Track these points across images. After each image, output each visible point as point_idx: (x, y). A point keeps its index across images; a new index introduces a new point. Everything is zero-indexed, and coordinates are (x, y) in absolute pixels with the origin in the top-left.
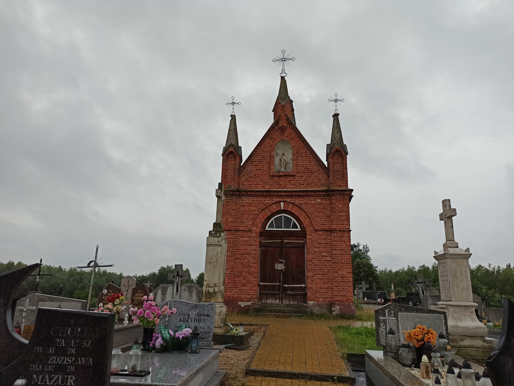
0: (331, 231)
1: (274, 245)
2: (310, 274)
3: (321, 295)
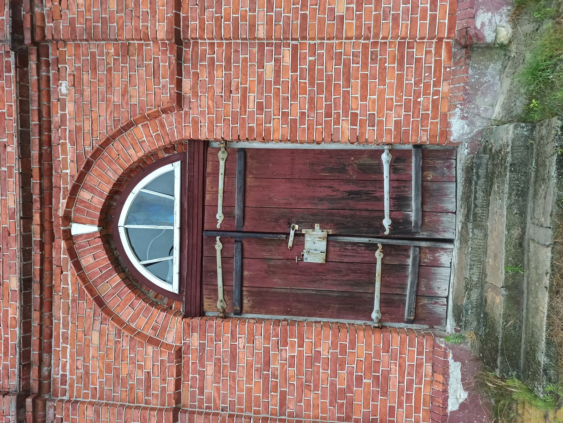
1: (236, 263)
2: (345, 128)
3: (427, 86)
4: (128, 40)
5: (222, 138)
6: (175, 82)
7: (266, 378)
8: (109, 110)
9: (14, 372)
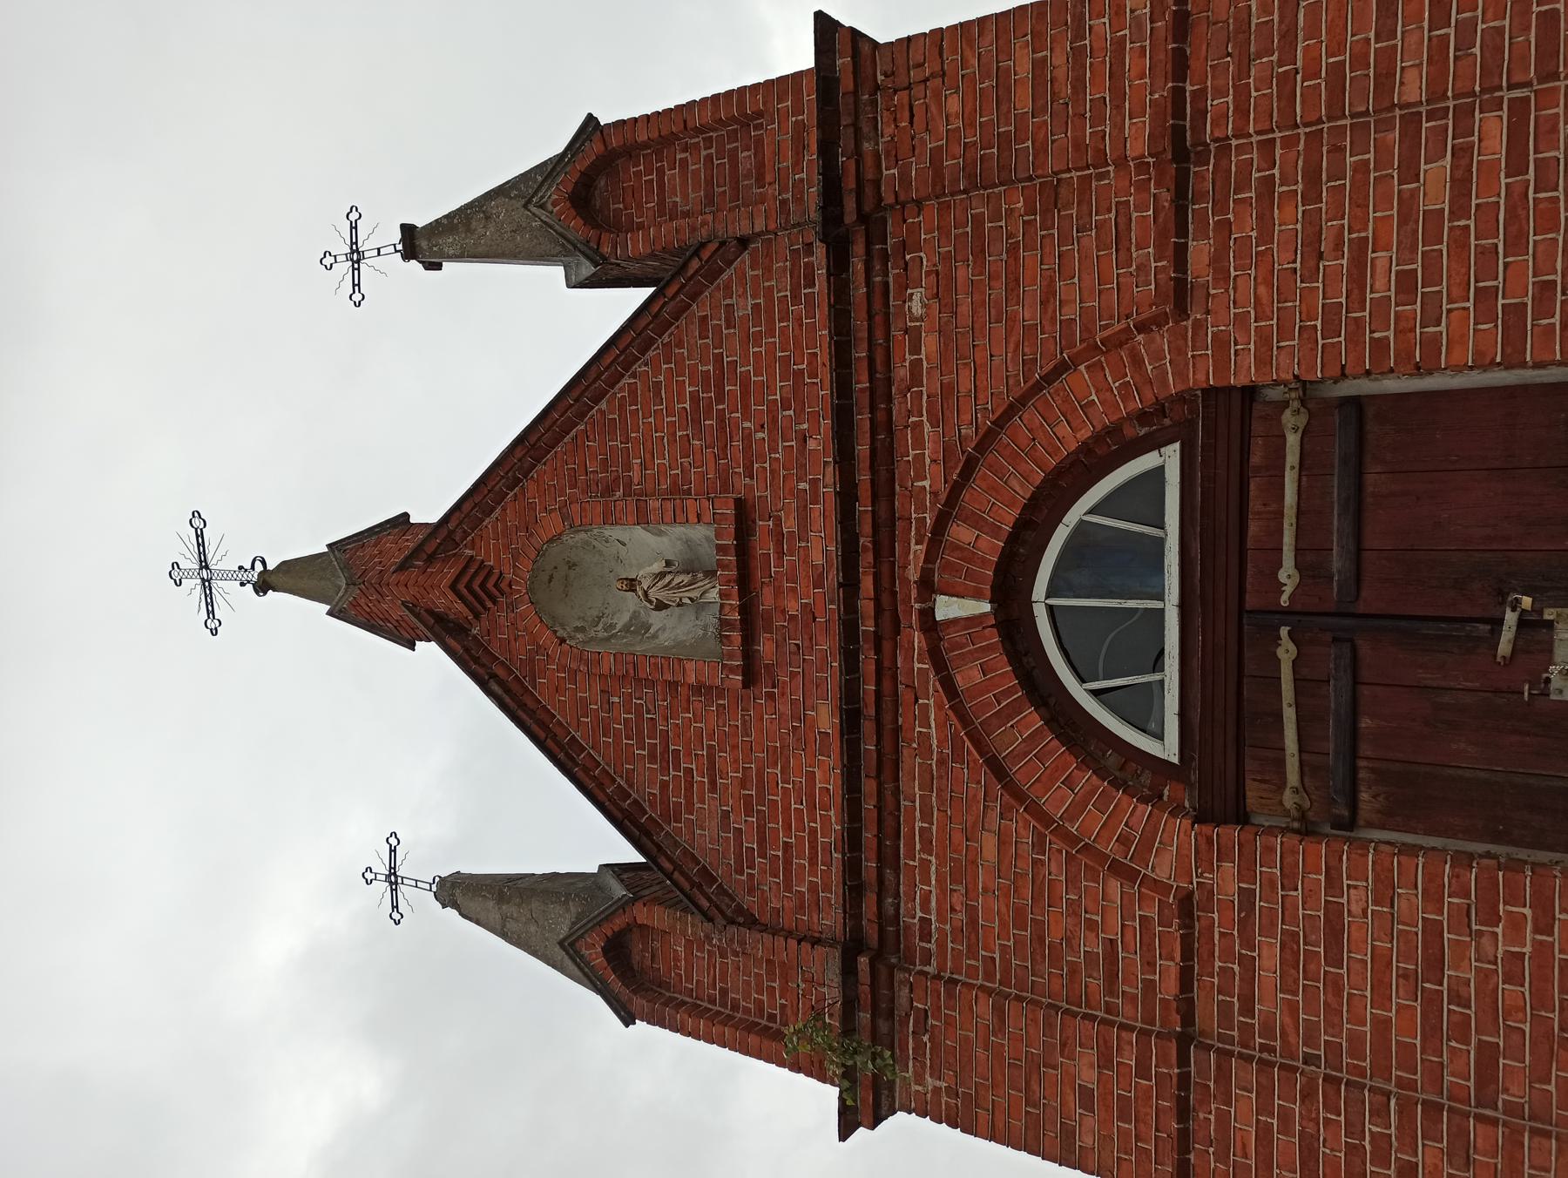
0: (1182, 155)
1: (1335, 696)
4: (1056, 173)
5: (1296, 377)
6: (1170, 251)
7: (1432, 1001)
8: (1013, 340)
9: (829, 899)
